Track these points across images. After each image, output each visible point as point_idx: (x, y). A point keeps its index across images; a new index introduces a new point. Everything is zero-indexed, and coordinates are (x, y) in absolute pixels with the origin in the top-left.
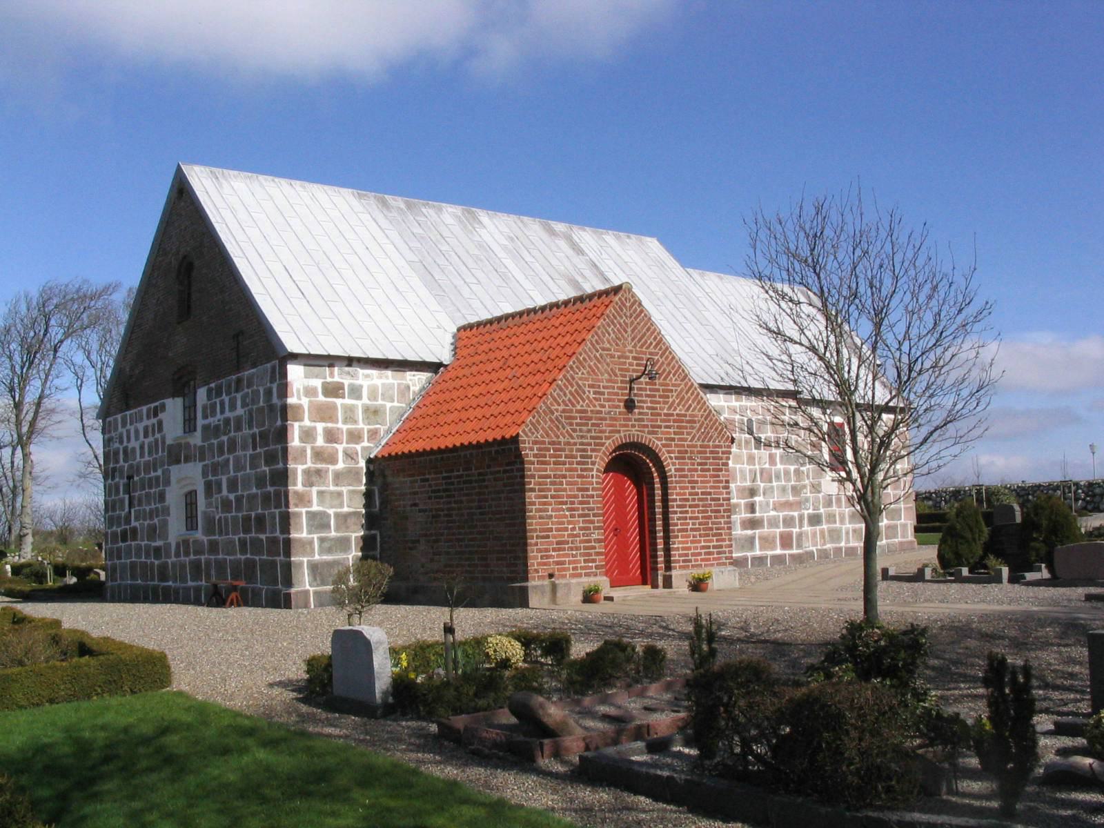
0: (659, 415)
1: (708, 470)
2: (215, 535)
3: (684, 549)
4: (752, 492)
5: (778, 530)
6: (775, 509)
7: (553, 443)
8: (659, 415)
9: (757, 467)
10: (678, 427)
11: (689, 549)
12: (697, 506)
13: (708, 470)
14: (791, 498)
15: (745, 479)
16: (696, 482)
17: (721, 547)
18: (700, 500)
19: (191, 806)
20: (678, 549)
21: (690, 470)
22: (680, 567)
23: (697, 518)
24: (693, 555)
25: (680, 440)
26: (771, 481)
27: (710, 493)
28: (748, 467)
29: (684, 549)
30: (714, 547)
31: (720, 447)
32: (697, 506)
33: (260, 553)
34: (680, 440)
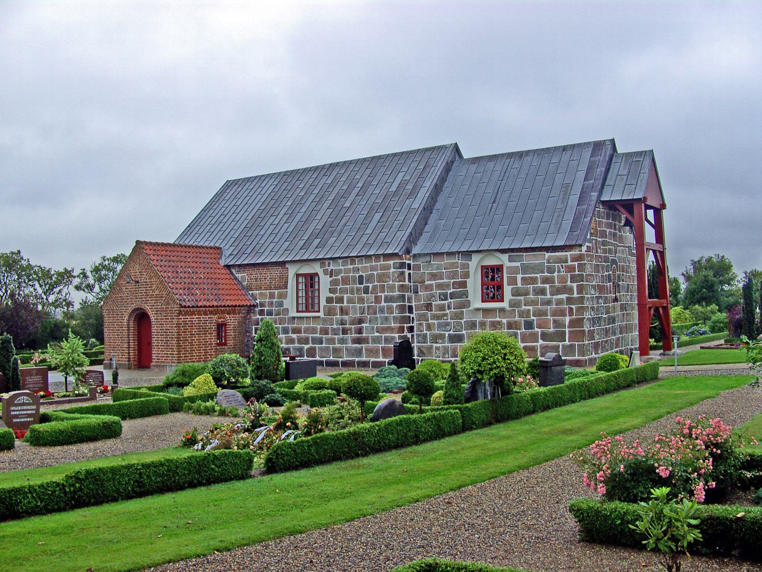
0: (148, 295)
1: (168, 319)
2: (565, 332)
3: (157, 354)
4: (361, 321)
5: (380, 346)
6: (378, 332)
7: (112, 310)
8: (148, 295)
9: (366, 305)
10: (156, 300)
11: (159, 354)
12: (163, 335)
13: (168, 319)
14: (393, 325)
15: (356, 313)
16: (163, 324)
17: (173, 354)
18: (165, 332)
19: (666, 553)
20: (155, 354)
21: (160, 319)
22: (197, 361)
23: (163, 340)
24: (161, 357)
25: (157, 306)
26: (375, 313)
27: (169, 330)
28: (358, 305)
29: (157, 354)
30: (170, 354)
31: (174, 308)
32: (163, 335)
33: (383, 349)
34: (157, 306)
